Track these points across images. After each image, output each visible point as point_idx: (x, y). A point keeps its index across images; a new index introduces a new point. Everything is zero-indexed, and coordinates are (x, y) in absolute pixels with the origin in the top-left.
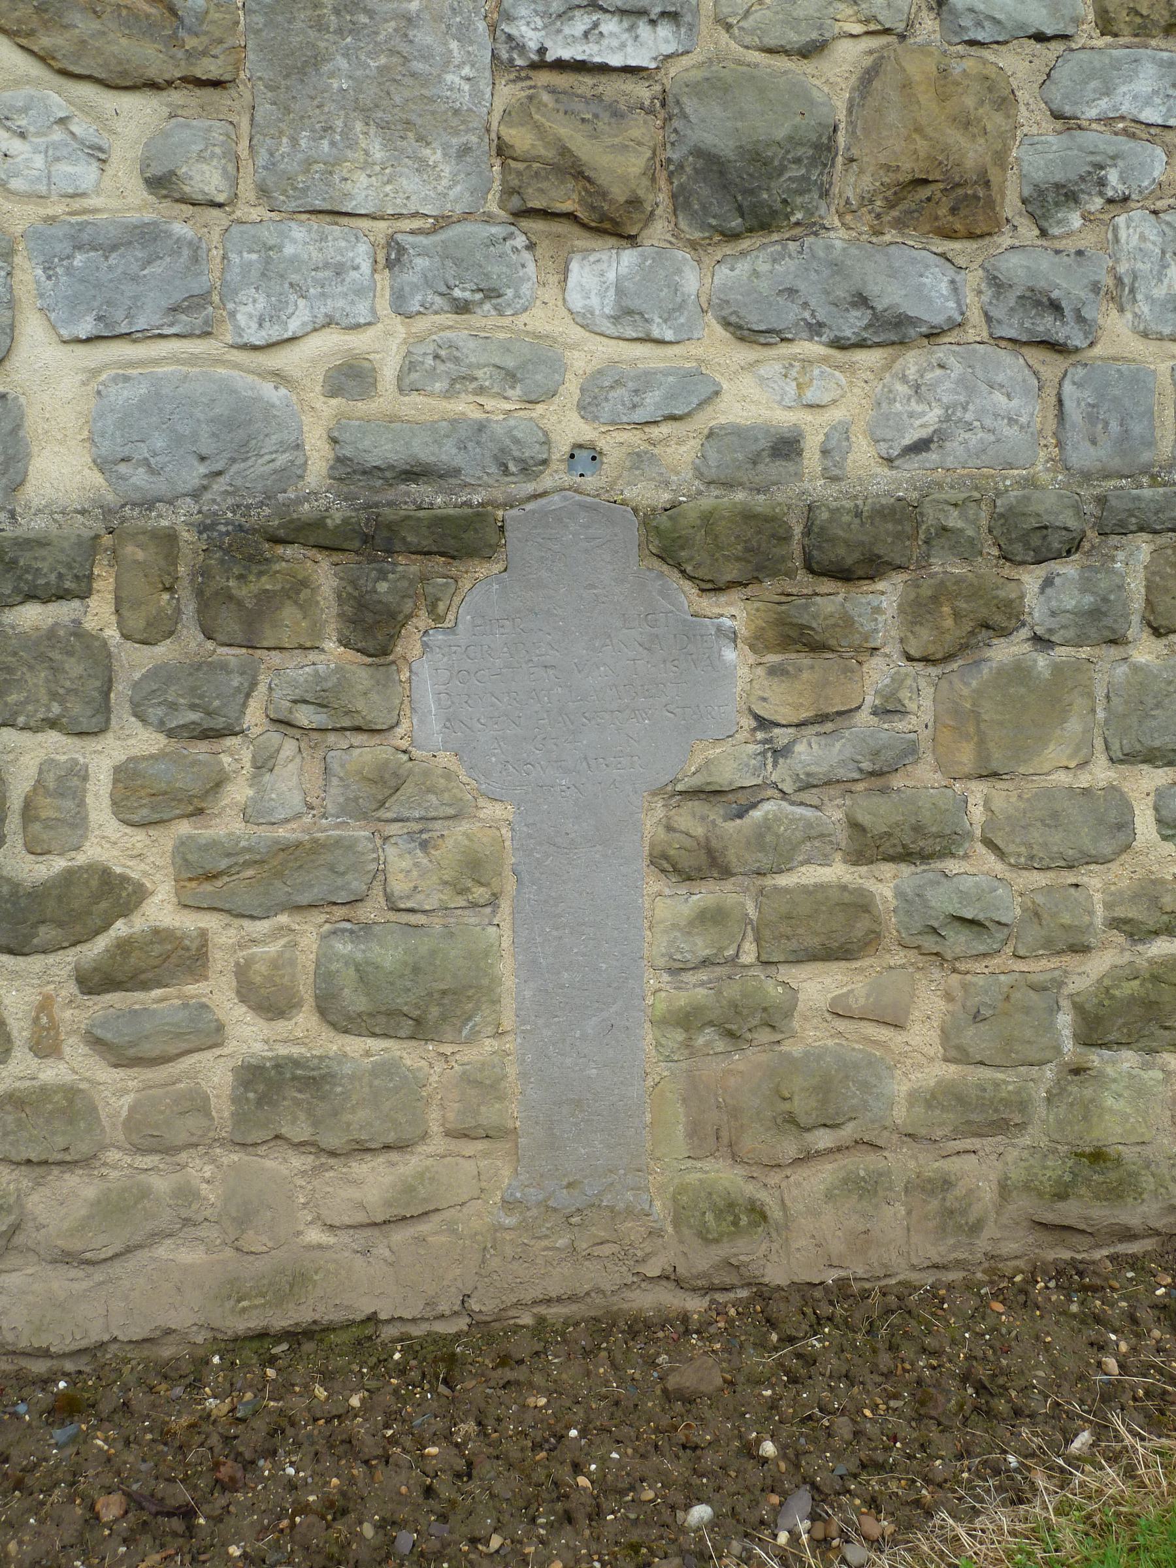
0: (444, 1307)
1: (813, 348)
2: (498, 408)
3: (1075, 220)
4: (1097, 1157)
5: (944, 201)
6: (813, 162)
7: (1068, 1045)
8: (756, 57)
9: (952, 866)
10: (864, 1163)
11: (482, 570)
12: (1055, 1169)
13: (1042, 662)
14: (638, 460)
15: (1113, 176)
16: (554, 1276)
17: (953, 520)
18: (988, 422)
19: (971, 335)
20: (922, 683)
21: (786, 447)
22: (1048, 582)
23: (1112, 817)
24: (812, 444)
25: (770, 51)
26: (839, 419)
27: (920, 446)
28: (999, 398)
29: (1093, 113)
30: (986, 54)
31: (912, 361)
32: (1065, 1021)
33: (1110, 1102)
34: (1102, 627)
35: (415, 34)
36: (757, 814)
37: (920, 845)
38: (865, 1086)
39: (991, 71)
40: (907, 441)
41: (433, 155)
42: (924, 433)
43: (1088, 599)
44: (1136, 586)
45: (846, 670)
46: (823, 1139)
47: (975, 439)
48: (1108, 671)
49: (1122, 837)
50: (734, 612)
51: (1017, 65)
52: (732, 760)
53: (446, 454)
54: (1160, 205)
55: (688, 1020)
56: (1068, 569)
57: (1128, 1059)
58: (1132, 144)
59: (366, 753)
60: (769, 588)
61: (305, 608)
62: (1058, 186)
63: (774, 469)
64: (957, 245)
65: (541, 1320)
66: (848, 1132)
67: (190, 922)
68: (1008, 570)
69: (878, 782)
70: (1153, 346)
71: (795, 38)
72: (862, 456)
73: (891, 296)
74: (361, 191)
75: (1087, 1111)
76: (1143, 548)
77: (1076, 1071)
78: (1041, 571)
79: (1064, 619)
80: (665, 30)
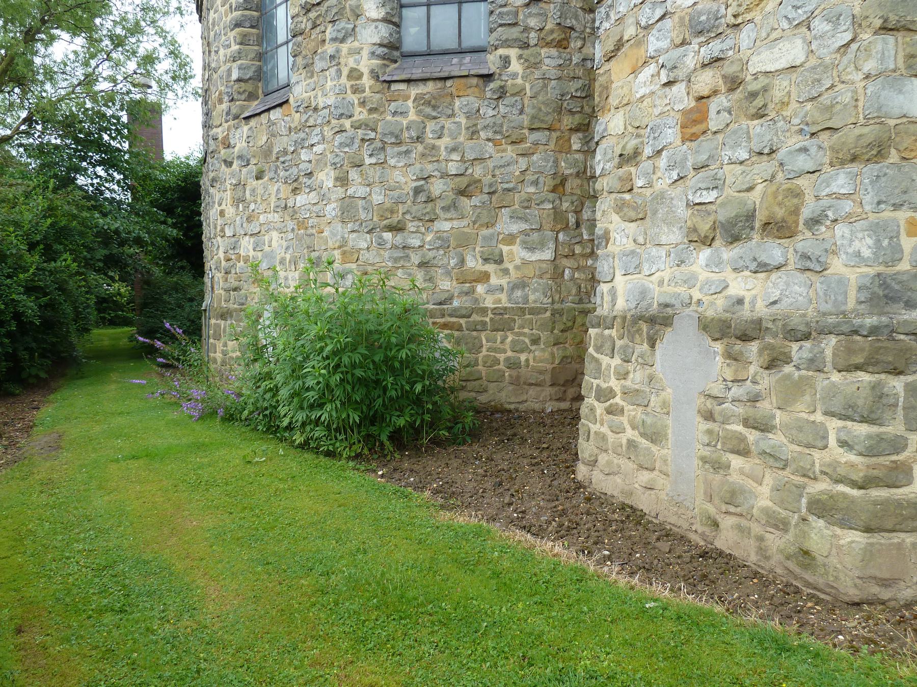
0: (652, 514)
1: (747, 273)
2: (680, 290)
3: (823, 229)
4: (806, 553)
5: (779, 228)
6: (747, 220)
7: (804, 510)
8: (736, 194)
9: (770, 436)
10: (744, 522)
11: (670, 329)
12: (792, 550)
13: (797, 374)
14: (712, 303)
15: (830, 213)
16: (671, 518)
17: (770, 325)
18: (793, 295)
19: (789, 268)
20: (765, 375)
21: (740, 301)
22: (801, 348)
23: (821, 433)
24: (747, 301)
25: (739, 192)
26: (754, 293)
27: (775, 303)
28: (796, 287)
29: (824, 194)
30: (794, 181)
31: (774, 276)
32: (804, 501)
33: (813, 535)
34: (815, 364)
35: (674, 202)
36: (724, 406)
37: (764, 427)
38: (745, 498)
39: (793, 187)
40: (771, 301)
41: (675, 229)
42: (776, 298)
43: (811, 355)
44: (829, 353)
45: (745, 368)
46: (732, 509)
47: (789, 301)
48: (821, 382)
49: (824, 442)
50: (718, 347)
51: (803, 182)
52: (717, 389)
53: (673, 301)
54: (851, 220)
55: (704, 460)
56: (807, 344)
57: (821, 523)
58: (839, 201)
59: (649, 370)
60: (725, 340)
61: (640, 335)
62: (811, 219)
63: (737, 307)
64: (783, 241)
65: (671, 530)
66: (738, 510)
67: (621, 403)
68: (787, 343)
69: (753, 404)
70: (849, 269)
71: (744, 187)
72: (760, 305)
73: (763, 258)
74: (664, 239)
75: (804, 535)
76: (833, 340)
77: (804, 520)
78: (799, 344)
79: (803, 361)
80: (715, 192)
